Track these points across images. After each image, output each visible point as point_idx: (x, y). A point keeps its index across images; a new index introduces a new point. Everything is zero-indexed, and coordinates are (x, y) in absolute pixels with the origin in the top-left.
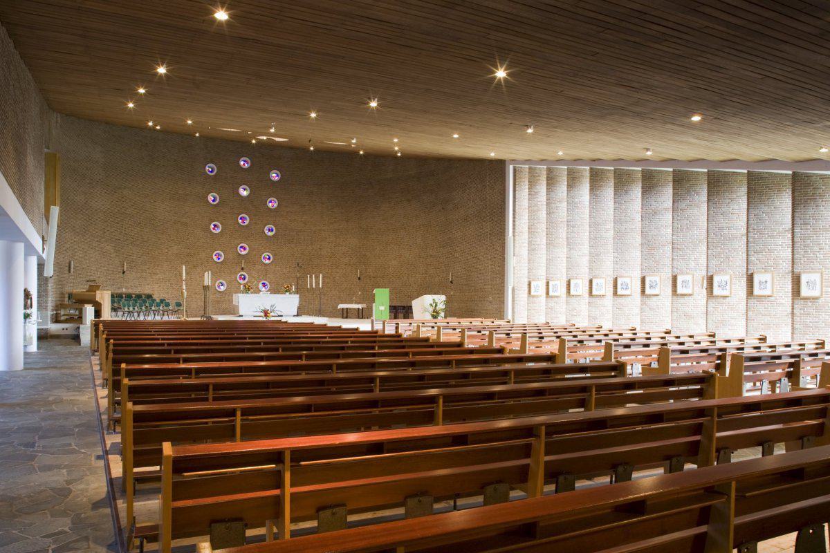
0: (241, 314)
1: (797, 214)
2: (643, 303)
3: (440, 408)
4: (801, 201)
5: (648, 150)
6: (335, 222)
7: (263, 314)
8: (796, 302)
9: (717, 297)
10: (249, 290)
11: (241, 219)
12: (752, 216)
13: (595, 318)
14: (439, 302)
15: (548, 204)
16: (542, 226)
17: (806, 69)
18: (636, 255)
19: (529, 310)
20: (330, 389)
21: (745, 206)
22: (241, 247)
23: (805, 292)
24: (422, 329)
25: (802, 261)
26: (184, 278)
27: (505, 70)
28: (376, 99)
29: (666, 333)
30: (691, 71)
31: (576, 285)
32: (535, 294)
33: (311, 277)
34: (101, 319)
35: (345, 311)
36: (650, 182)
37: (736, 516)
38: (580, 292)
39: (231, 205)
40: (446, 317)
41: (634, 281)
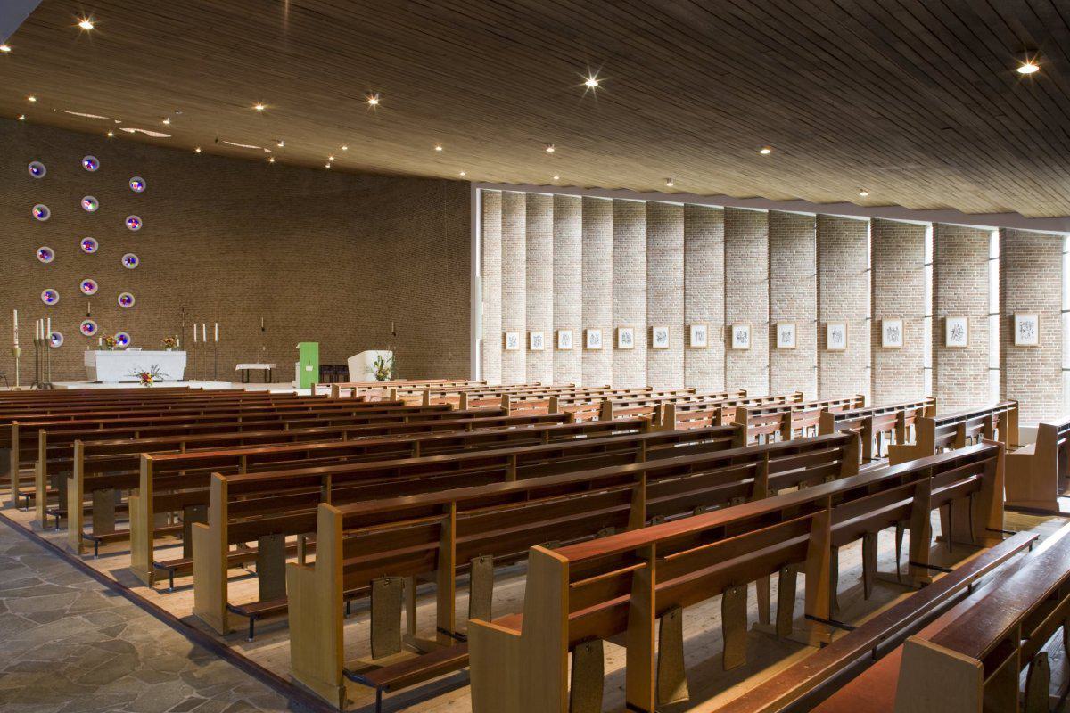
0: (99, 380)
1: (823, 261)
2: (649, 358)
3: (328, 491)
5: (669, 180)
6: (227, 252)
7: (140, 379)
8: (823, 355)
9: (737, 350)
10: (112, 346)
11: (85, 243)
12: (774, 261)
13: (590, 376)
14: (385, 359)
15: (529, 238)
16: (521, 266)
17: (922, 111)
18: (640, 302)
19: (504, 368)
20: (177, 474)
21: (765, 249)
22: (86, 284)
23: (831, 345)
24: (397, 395)
27: (596, 79)
28: (377, 95)
29: (690, 392)
31: (565, 337)
32: (512, 348)
33: (200, 328)
35: (245, 373)
36: (657, 219)
37: (657, 583)
38: (569, 346)
39: (68, 224)
40: (392, 379)
41: (637, 333)
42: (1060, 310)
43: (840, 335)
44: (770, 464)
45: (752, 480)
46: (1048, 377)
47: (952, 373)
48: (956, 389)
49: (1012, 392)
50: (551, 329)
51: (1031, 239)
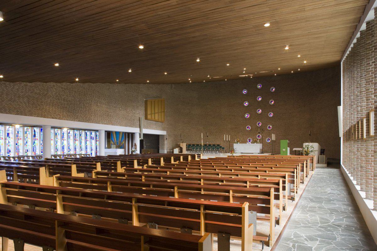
26: (202, 140)
34: (182, 153)
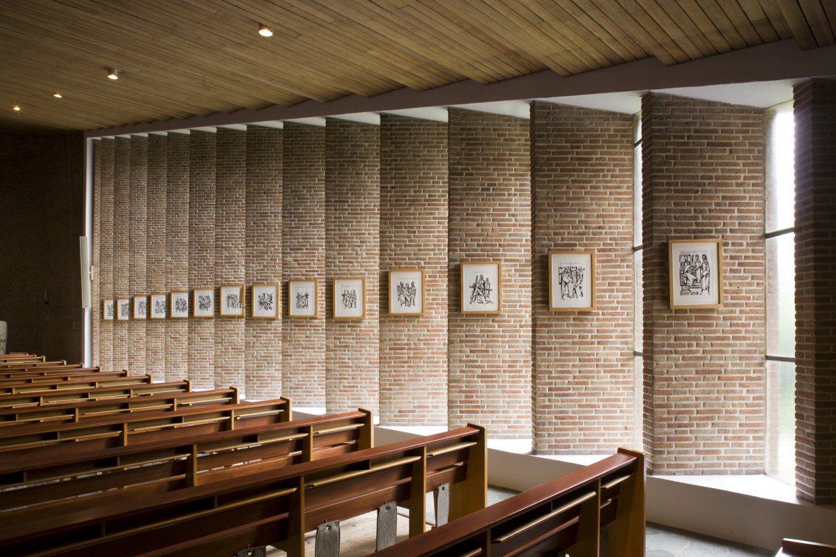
4: (335, 165)
25: (337, 260)
30: (174, 16)
42: (629, 247)
43: (353, 296)
44: (198, 474)
45: (286, 515)
46: (609, 368)
47: (473, 357)
48: (480, 384)
49: (545, 395)
50: (524, 253)
51: (580, 119)
